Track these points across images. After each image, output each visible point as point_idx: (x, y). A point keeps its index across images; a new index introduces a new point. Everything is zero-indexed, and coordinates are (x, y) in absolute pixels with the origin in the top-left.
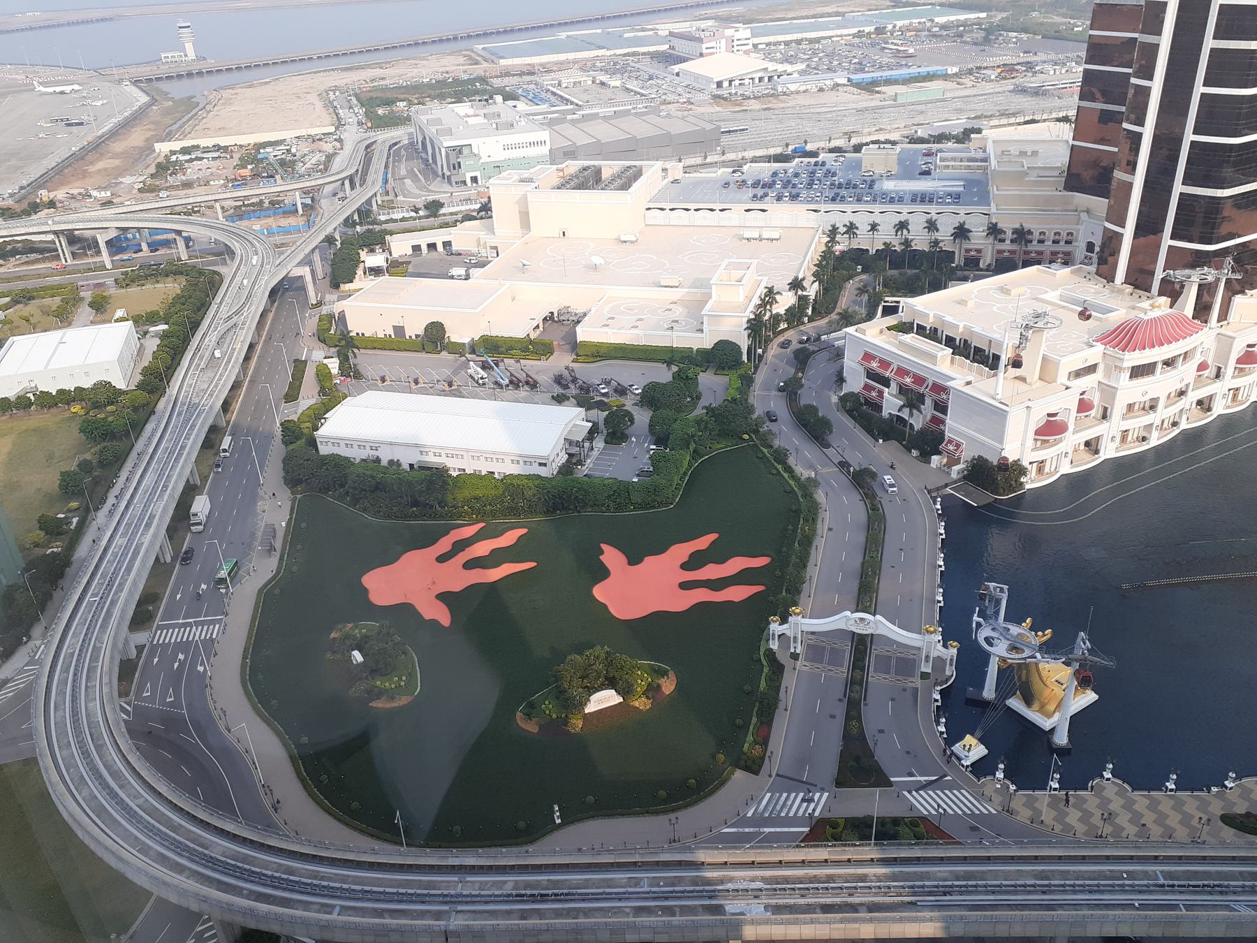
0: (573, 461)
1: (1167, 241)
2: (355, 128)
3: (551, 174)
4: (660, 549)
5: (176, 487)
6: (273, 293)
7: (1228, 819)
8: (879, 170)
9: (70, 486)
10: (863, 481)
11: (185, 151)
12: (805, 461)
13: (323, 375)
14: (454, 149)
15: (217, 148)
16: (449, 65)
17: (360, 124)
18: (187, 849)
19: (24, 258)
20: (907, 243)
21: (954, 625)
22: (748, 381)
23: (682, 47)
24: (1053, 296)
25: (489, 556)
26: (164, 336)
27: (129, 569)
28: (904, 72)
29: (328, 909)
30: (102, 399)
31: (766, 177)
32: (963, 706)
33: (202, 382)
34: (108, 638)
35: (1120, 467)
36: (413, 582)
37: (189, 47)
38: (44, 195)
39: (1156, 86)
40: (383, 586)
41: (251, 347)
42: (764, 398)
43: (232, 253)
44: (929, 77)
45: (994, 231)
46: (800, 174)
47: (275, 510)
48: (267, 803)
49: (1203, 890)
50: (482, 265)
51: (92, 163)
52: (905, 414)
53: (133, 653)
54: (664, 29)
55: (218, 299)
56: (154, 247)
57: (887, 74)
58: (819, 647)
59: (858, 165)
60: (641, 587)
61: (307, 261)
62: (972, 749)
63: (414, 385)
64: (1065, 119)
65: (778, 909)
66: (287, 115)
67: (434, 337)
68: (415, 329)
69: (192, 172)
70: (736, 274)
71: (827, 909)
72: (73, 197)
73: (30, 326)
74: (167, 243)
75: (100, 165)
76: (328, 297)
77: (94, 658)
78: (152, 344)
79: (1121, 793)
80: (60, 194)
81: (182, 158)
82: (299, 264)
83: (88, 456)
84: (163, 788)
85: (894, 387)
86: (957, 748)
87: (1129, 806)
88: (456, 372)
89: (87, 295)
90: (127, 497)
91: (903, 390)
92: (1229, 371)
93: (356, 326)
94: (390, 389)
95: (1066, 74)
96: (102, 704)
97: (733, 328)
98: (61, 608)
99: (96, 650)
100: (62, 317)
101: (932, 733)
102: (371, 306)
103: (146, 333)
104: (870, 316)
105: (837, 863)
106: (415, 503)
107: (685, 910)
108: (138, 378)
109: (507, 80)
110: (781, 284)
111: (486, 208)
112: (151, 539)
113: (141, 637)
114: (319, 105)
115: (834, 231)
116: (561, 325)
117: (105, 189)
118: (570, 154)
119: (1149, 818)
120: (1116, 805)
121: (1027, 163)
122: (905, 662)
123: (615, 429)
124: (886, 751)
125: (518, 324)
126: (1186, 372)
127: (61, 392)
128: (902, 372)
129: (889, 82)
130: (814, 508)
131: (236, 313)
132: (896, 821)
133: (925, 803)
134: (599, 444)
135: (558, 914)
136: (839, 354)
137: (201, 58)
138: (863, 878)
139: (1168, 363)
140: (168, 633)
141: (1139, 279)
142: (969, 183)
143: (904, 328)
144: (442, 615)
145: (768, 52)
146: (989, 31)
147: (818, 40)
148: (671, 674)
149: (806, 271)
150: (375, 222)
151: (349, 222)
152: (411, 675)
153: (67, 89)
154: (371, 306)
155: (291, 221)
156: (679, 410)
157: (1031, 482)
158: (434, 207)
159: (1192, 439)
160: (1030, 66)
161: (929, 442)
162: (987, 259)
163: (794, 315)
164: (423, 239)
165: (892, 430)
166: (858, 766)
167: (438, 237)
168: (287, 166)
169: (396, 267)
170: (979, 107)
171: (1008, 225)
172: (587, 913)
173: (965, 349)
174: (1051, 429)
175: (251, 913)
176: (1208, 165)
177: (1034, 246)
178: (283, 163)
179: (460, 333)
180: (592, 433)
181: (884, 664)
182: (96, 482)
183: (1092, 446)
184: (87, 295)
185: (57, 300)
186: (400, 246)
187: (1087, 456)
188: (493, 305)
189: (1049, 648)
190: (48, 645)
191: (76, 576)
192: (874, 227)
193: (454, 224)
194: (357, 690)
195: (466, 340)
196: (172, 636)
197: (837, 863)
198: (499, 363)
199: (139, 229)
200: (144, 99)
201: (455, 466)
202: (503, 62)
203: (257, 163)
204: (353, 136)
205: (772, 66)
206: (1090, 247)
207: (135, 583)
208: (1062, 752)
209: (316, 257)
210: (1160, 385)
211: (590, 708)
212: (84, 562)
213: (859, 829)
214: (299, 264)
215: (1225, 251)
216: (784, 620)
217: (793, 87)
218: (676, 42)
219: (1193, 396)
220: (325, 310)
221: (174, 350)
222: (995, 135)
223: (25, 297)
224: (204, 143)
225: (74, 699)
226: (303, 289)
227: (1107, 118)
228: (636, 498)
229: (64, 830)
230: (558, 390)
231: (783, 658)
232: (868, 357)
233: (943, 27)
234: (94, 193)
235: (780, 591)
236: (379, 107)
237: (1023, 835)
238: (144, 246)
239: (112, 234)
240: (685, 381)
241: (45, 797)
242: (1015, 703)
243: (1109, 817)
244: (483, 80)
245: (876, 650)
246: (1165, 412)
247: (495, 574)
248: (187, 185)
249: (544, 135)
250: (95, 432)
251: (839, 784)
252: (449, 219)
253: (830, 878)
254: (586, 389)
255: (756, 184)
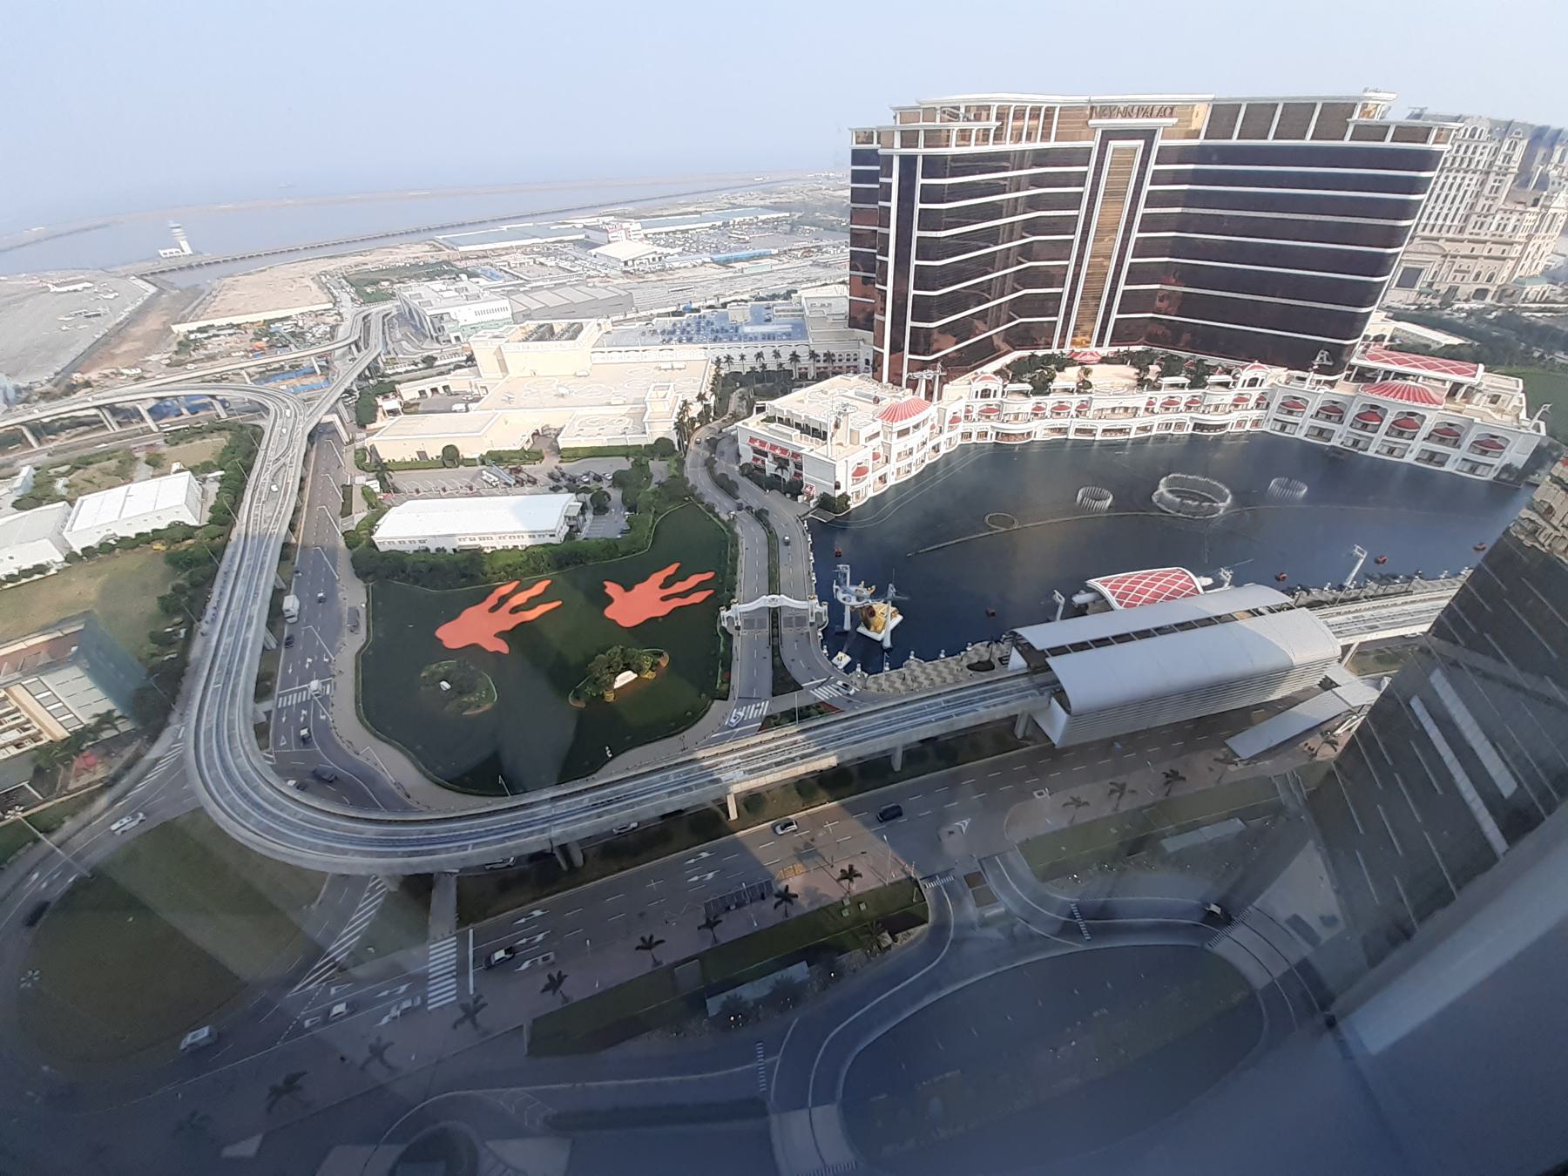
0: (573, 531)
1: (907, 356)
2: (350, 304)
3: (517, 332)
4: (645, 579)
5: (265, 593)
6: (310, 436)
7: (970, 667)
8: (740, 319)
9: (169, 607)
10: (761, 516)
11: (200, 330)
12: (724, 508)
13: (367, 493)
14: (436, 316)
15: (232, 326)
16: (417, 252)
17: (353, 300)
18: (345, 838)
19: (74, 432)
20: (764, 366)
21: (825, 594)
22: (681, 463)
23: (595, 236)
24: (851, 393)
25: (530, 602)
26: (222, 480)
27: (242, 659)
28: (744, 253)
29: (465, 848)
30: (180, 536)
31: (669, 327)
32: (834, 638)
33: (265, 514)
34: (238, 713)
35: (898, 488)
36: (475, 628)
37: (184, 245)
38: (77, 377)
39: (891, 260)
40: (453, 635)
41: (302, 480)
42: (697, 477)
43: (267, 410)
44: (761, 256)
45: (813, 355)
46: (692, 325)
47: (353, 596)
48: (401, 794)
49: (962, 705)
50: (477, 400)
51: (116, 347)
52: (779, 473)
53: (264, 718)
54: (579, 223)
55: (263, 446)
56: (194, 410)
57: (735, 254)
58: (750, 620)
59: (726, 317)
60: (635, 605)
61: (333, 410)
62: (843, 659)
63: (442, 493)
64: (843, 282)
65: (751, 771)
66: (291, 295)
67: (451, 457)
68: (434, 452)
69: (213, 346)
70: (661, 394)
71: (778, 764)
72: (107, 376)
73: (94, 486)
74: (205, 406)
75: (124, 348)
76: (359, 436)
77: (231, 728)
78: (213, 488)
79: (920, 665)
80: (93, 375)
81: (199, 336)
82: (328, 412)
83: (180, 582)
84: (316, 804)
85: (770, 457)
86: (835, 660)
87: (923, 672)
88: (473, 479)
89: (141, 455)
90: (224, 606)
91: (776, 458)
92: (946, 429)
93: (386, 456)
94: (451, 496)
95: (840, 253)
96: (247, 757)
97: (663, 428)
98: (189, 698)
99: (231, 722)
100: (123, 474)
101: (820, 655)
102: (394, 438)
103: (204, 480)
104: (750, 414)
105: (780, 738)
106: (464, 576)
107: (697, 786)
108: (208, 515)
109: (469, 263)
110: (691, 398)
111: (471, 358)
112: (256, 633)
113: (267, 705)
114: (314, 287)
115: (718, 360)
116: (544, 442)
117: (135, 367)
118: (528, 316)
119: (934, 675)
120: (918, 672)
121: (826, 311)
122: (800, 619)
123: (599, 505)
124: (797, 670)
125: (513, 439)
126: (925, 431)
127: (154, 531)
128: (773, 447)
129: (737, 260)
130: (735, 537)
131: (283, 455)
132: (808, 707)
133: (823, 694)
134: (589, 516)
135: (620, 809)
136: (735, 439)
137: (196, 253)
138: (795, 743)
139: (916, 427)
140: (286, 699)
141: (895, 379)
142: (795, 326)
143: (770, 420)
144: (504, 648)
145: (655, 239)
146: (793, 225)
147: (687, 231)
148: (666, 655)
149: (706, 389)
150: (383, 376)
151: (361, 377)
152: (488, 689)
153: (79, 287)
154: (394, 438)
155: (312, 379)
156: (639, 487)
157: (853, 504)
158: (429, 361)
159: (932, 467)
160: (819, 248)
161: (794, 489)
162: (812, 373)
163: (704, 417)
164: (426, 385)
165: (773, 484)
166: (783, 682)
167: (439, 383)
168: (298, 336)
169: (409, 408)
170: (794, 276)
171: (820, 352)
172: (638, 803)
173: (806, 429)
174: (860, 472)
175: (409, 865)
176: (924, 309)
177: (837, 364)
178: (293, 334)
179: (469, 451)
180: (583, 510)
181: (789, 622)
182: (192, 599)
183: (883, 479)
184: (141, 455)
185: (114, 462)
186: (409, 392)
187: (880, 485)
188: (479, 433)
189: (874, 596)
190: (187, 726)
191: (196, 673)
192: (742, 357)
193: (449, 372)
194: (450, 707)
195: (476, 456)
196: (294, 699)
197: (780, 738)
198: (511, 468)
199: (176, 397)
200: (152, 290)
201: (487, 546)
202: (461, 249)
203: (268, 335)
204: (349, 308)
205: (660, 250)
206: (867, 362)
207: (250, 667)
208: (889, 650)
209: (340, 405)
210: (913, 440)
211: (617, 686)
212: (200, 661)
213: (791, 716)
214: (328, 412)
215: (936, 360)
216: (728, 608)
217: (676, 265)
218: (589, 232)
219: (930, 444)
220: (358, 445)
221: (234, 488)
222: (806, 294)
223: (85, 462)
224: (217, 322)
225: (222, 760)
226: (335, 431)
227: (866, 281)
228: (622, 548)
229: (243, 850)
230: (553, 484)
231: (731, 630)
232: (752, 440)
233: (764, 222)
234: (126, 371)
235: (723, 592)
236: (367, 286)
237: (873, 699)
238: (184, 411)
239: (153, 403)
240: (640, 467)
241: (219, 831)
242: (862, 630)
243: (915, 679)
244: (448, 263)
245: (784, 615)
246: (917, 456)
247: (531, 615)
248: (212, 358)
249: (505, 303)
250: (178, 562)
251: (774, 695)
252: (443, 369)
253: (778, 747)
254: (573, 480)
255: (663, 332)
